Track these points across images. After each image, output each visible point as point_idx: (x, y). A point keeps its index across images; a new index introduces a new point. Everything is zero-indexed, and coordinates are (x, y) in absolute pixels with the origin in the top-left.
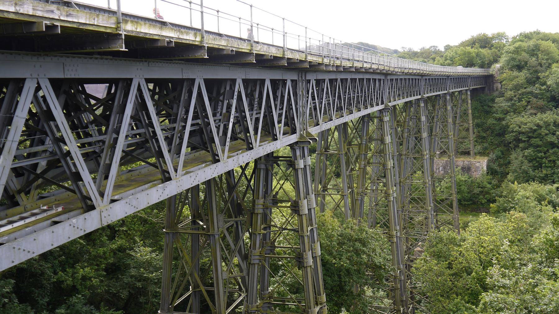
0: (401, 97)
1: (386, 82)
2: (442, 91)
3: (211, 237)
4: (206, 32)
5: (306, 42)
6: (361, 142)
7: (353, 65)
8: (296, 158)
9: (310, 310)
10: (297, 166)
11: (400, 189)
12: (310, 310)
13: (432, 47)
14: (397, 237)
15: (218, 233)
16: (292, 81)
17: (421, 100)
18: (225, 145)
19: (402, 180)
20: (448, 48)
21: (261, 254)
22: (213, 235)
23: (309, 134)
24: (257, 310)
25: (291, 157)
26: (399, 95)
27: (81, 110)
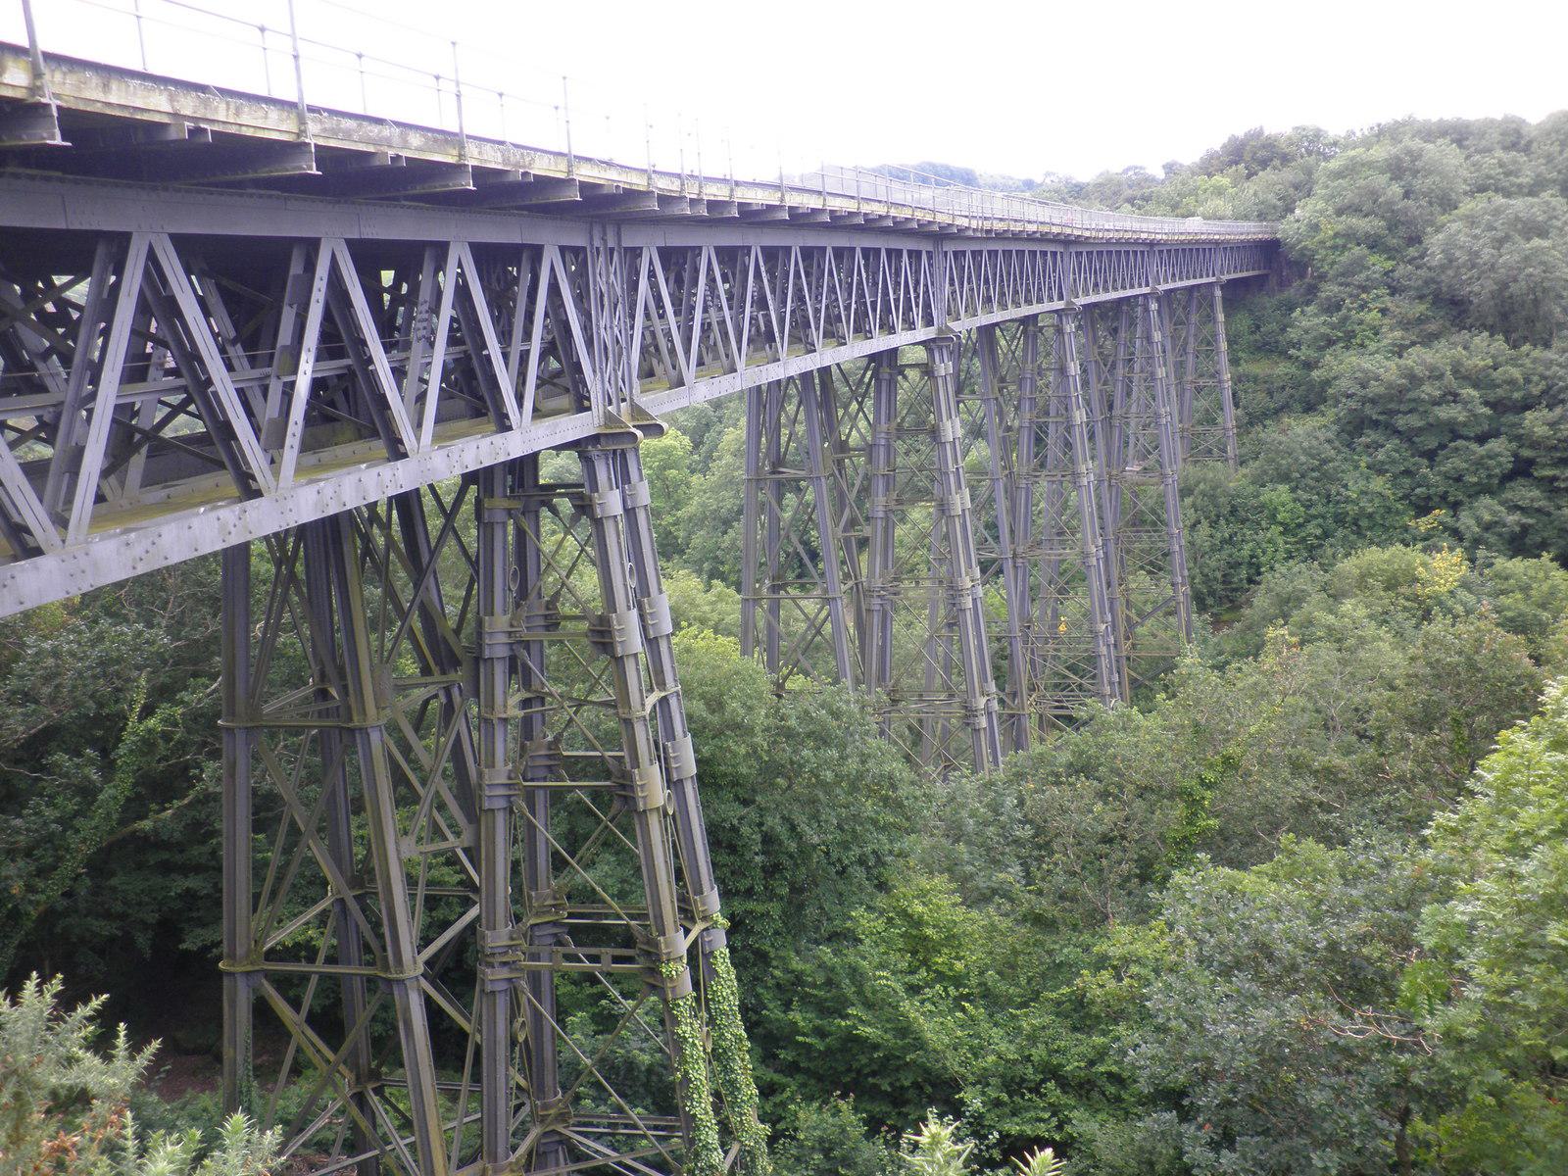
0: (995, 305)
1: (938, 259)
2: (1040, 300)
3: (358, 735)
4: (48, 56)
5: (296, 57)
6: (874, 437)
7: (782, 200)
8: (595, 487)
9: (661, 939)
10: (598, 510)
12: (661, 939)
13: (1128, 169)
14: (989, 714)
15: (380, 723)
16: (928, 252)
17: (940, 349)
18: (282, 446)
19: (1020, 550)
20: (1170, 168)
21: (510, 778)
22: (364, 731)
23: (637, 411)
24: (510, 947)
25: (582, 486)
26: (833, 320)
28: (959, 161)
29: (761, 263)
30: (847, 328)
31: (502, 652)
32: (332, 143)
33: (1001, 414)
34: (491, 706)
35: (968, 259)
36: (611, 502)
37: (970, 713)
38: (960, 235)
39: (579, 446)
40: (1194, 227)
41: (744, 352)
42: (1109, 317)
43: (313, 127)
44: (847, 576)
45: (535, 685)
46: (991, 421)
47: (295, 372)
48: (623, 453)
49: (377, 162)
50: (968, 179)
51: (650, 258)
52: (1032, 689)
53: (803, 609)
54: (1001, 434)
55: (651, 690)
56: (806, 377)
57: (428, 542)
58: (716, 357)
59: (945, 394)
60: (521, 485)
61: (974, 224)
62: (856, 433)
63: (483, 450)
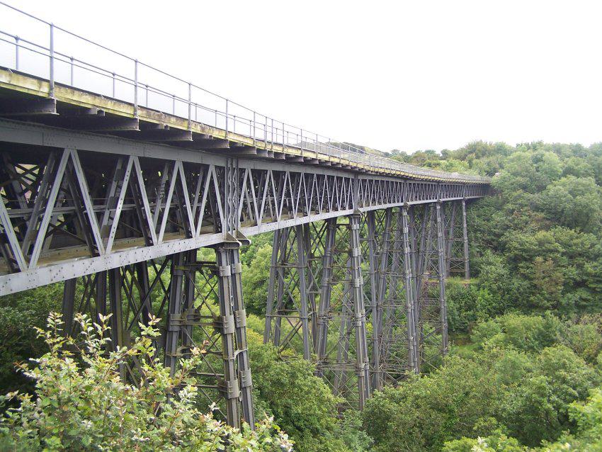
2: (394, 202)
4: (56, 83)
8: (220, 264)
11: (377, 315)
14: (366, 371)
23: (239, 235)
26: (315, 203)
27: (9, 178)
28: (358, 142)
29: (272, 177)
30: (319, 207)
31: (177, 329)
32: (145, 119)
33: (375, 248)
34: (170, 351)
35: (367, 184)
36: (227, 270)
37: (358, 369)
38: (366, 173)
39: (215, 247)
40: (455, 176)
41: (261, 217)
42: (419, 213)
43: (139, 112)
44: (310, 310)
45: (188, 344)
46: (370, 251)
47: (116, 207)
48: (232, 251)
49: (160, 127)
50: (362, 150)
51: (248, 173)
52: (381, 362)
53: (287, 325)
54: (374, 255)
55: (236, 349)
56: (298, 227)
57: (148, 284)
58: (249, 218)
59: (356, 237)
60: (189, 261)
61: (269, 148)
62: (318, 251)
63: (179, 246)
